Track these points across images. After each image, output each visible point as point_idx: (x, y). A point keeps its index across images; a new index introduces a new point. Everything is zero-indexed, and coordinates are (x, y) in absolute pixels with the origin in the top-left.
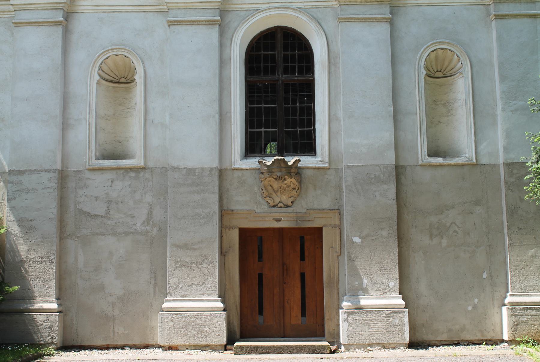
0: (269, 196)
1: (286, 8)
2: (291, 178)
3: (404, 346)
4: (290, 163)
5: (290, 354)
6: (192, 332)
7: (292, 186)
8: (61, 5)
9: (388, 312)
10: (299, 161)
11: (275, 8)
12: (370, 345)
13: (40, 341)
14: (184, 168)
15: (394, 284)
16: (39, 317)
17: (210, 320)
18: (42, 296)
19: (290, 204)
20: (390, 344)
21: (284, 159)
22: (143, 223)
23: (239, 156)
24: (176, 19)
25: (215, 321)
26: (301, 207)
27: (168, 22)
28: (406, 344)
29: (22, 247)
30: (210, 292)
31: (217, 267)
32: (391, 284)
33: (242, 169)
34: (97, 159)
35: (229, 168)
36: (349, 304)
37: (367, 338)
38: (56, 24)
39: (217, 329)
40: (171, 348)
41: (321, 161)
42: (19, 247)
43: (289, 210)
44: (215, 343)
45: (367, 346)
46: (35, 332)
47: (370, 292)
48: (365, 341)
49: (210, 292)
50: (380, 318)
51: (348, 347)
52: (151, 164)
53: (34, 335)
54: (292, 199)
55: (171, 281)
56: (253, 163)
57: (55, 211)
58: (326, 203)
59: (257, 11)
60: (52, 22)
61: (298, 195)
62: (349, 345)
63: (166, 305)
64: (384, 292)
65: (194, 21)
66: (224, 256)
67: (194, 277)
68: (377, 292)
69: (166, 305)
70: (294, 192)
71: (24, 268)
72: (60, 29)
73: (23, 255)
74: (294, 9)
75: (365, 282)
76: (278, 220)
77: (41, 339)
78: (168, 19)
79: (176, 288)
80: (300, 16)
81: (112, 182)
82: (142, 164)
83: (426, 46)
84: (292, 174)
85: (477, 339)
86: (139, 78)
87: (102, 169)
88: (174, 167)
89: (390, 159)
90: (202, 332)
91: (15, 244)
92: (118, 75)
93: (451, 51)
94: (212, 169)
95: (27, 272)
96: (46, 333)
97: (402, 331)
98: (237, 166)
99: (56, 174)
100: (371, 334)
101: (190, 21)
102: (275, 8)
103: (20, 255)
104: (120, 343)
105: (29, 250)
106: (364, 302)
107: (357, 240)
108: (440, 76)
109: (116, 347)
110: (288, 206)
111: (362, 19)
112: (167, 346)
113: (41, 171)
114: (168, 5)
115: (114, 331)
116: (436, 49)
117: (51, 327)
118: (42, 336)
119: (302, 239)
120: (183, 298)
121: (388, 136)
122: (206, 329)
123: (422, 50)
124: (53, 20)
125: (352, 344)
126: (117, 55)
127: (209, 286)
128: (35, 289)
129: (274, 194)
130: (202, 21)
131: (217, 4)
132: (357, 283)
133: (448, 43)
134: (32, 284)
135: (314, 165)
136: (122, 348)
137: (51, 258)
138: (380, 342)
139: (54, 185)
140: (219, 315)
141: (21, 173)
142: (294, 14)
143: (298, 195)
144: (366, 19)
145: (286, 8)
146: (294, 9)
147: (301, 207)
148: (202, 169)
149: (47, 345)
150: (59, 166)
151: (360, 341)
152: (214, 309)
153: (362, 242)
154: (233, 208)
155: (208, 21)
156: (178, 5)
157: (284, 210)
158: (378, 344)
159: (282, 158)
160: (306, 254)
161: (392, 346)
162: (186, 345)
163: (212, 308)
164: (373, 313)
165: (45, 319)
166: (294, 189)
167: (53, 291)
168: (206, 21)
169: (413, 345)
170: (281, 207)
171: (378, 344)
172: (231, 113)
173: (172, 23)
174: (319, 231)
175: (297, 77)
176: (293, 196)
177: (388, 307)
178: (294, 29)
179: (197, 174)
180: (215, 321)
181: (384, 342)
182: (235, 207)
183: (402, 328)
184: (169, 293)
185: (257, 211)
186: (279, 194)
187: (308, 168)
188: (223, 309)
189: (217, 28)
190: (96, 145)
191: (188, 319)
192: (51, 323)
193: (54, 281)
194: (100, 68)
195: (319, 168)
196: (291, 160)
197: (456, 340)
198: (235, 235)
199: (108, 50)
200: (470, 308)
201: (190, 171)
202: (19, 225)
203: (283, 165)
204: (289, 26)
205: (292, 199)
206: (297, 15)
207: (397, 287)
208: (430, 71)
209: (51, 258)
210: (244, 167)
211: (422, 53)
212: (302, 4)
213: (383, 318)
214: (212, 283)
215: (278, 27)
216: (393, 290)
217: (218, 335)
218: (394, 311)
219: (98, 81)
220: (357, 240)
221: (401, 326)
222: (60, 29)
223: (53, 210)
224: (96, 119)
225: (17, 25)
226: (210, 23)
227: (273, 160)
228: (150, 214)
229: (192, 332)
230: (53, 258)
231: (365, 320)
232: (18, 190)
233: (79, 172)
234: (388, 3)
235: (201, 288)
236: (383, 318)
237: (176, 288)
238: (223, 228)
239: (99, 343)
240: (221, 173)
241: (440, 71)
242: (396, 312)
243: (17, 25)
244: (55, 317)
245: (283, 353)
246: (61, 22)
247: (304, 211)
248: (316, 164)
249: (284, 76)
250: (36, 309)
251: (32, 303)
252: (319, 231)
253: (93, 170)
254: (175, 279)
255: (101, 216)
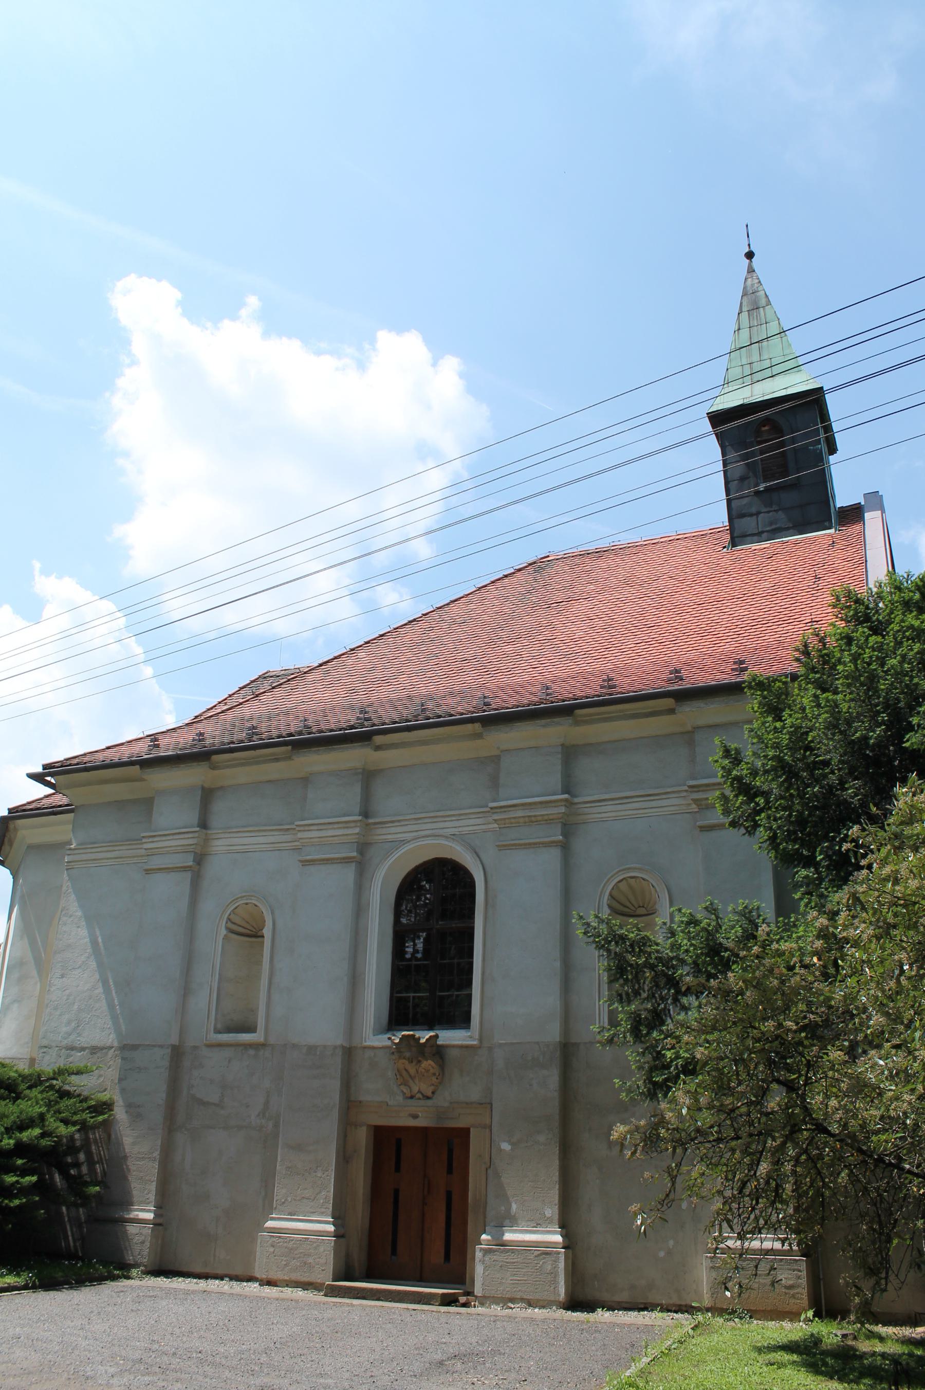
0: (405, 1084)
1: (436, 836)
2: (427, 1060)
3: (557, 1306)
4: (423, 1041)
5: (390, 1301)
6: (294, 1263)
7: (432, 1071)
8: (192, 847)
9: (536, 1253)
10: (437, 1036)
11: (423, 837)
12: (512, 1300)
13: (129, 1260)
14: (305, 1046)
15: (552, 1211)
16: (132, 1229)
17: (316, 1248)
18: (140, 1203)
19: (430, 1094)
20: (538, 1300)
21: (413, 1036)
22: (258, 1115)
23: (371, 1031)
24: (309, 858)
25: (322, 1249)
26: (443, 1099)
27: (301, 861)
28: (560, 1302)
29: (127, 1138)
30: (323, 1210)
31: (333, 1176)
32: (548, 1213)
33: (373, 1048)
34: (218, 1031)
35: (359, 1045)
36: (489, 1237)
37: (508, 1289)
38: (185, 869)
39: (323, 1261)
40: (270, 1283)
41: (471, 1037)
42: (124, 1138)
43: (429, 1102)
44: (319, 1281)
45: (507, 1301)
46: (126, 1248)
47: (520, 1222)
48: (505, 1293)
49: (323, 1210)
50: (527, 1261)
51: (484, 1301)
52: (272, 1041)
53: (125, 1252)
54: (432, 1087)
55: (279, 1192)
56: (382, 1040)
57: (164, 1095)
58: (475, 1094)
59: (404, 842)
60: (182, 867)
61: (440, 1083)
62: (484, 1297)
63: (270, 1224)
64: (538, 1223)
65: (328, 860)
66: (347, 1162)
67: (306, 1189)
68: (529, 1223)
69: (270, 1224)
70: (434, 1079)
71: (127, 1166)
72: (188, 875)
73: (128, 1149)
74: (446, 837)
75: (514, 1206)
76: (415, 1117)
77: (131, 1258)
78: (301, 858)
79: (284, 1203)
80: (453, 845)
81: (229, 1061)
82: (262, 1040)
83: (612, 874)
84: (426, 1054)
85: (671, 1303)
86: (267, 932)
87: (220, 1045)
88: (293, 1044)
89: (553, 1033)
90: (305, 1263)
91: (121, 1135)
92: (255, 926)
93: (644, 879)
94: (335, 1047)
95: (129, 1170)
96: (137, 1249)
97: (555, 1282)
98: (368, 1043)
99: (169, 1050)
100: (513, 1284)
101: (323, 860)
102: (423, 837)
103: (124, 1149)
104: (220, 1272)
105: (134, 1144)
106: (508, 1236)
107: (506, 1146)
108: (643, 913)
109: (215, 1277)
110: (428, 1098)
111: (525, 844)
112: (265, 1281)
113: (154, 1046)
114: (301, 841)
115: (215, 1256)
116: (624, 879)
117: (143, 1242)
118: (132, 1253)
119: (399, 1143)
120: (292, 1215)
121: (553, 1001)
122: (310, 1260)
123: (606, 880)
124: (181, 865)
125: (489, 1297)
126: (247, 904)
127: (322, 1201)
128: (135, 1193)
129: (411, 1081)
130: (337, 859)
131: (354, 837)
132: (503, 1208)
133: (640, 870)
134: (132, 1186)
135: (460, 1043)
136: (221, 1278)
137: (154, 1155)
138: (525, 1297)
139: (166, 1063)
140: (327, 1242)
141: (135, 1047)
142: (446, 843)
143: (440, 1083)
144: (530, 844)
145: (436, 836)
146: (446, 837)
147: (443, 1099)
148: (325, 1047)
149: (135, 1266)
150: (174, 1040)
151: (498, 1292)
152: (322, 1234)
153: (512, 1149)
154: (361, 1098)
155: (344, 858)
156: (312, 840)
157: (422, 1102)
158: (522, 1300)
159: (411, 1033)
160: (455, 1164)
161: (541, 1303)
162: (286, 1281)
163: (320, 1231)
164: (517, 1253)
165: (137, 1231)
166: (434, 1074)
167: (152, 1197)
168: (341, 859)
169: (575, 1303)
170: (419, 1099)
171: (522, 1300)
172: (365, 974)
173: (306, 863)
174: (464, 1133)
175: (455, 924)
176: (433, 1085)
177: (540, 1245)
178: (455, 861)
179: (318, 1053)
180: (322, 1249)
181: (531, 1297)
182: (365, 1097)
183: (555, 1277)
184: (276, 1208)
185: (389, 1103)
186: (417, 1081)
187: (454, 1046)
188: (333, 1235)
189: (353, 866)
190: (216, 1014)
191: (290, 1245)
192: (143, 1238)
193: (154, 1183)
194: (229, 919)
195: (467, 1047)
196: (424, 1036)
197: (642, 1303)
198: (362, 1138)
199: (237, 899)
200: (662, 1254)
201: (311, 1049)
202: (126, 1112)
203: (412, 1042)
204: (449, 857)
205: (432, 1087)
206: (450, 844)
207: (556, 1217)
208: (628, 907)
209: (154, 1155)
210: (376, 1044)
211: (605, 885)
212: (456, 830)
213: (530, 1261)
214: (326, 1198)
215: (437, 859)
216: (550, 1221)
217: (323, 1270)
218: (545, 1250)
219: (225, 935)
220: (506, 1146)
221: (554, 1274)
222: (188, 875)
223: (161, 1096)
224: (219, 982)
225: (148, 871)
226: (346, 861)
227: (427, 1037)
228: (267, 1103)
229: (294, 1263)
230: (156, 1154)
231: (507, 1263)
232: (130, 1069)
233: (195, 1048)
234: (558, 821)
235: (312, 1204)
236: (530, 1261)
237: (284, 1203)
238: (347, 1123)
239: (198, 1269)
240: (349, 1053)
241: (643, 907)
242: (547, 1253)
243: (148, 871)
244: (148, 1230)
245: (382, 1300)
246: (190, 867)
247: (446, 1104)
248: (464, 1040)
249: (440, 923)
250: (130, 1218)
251: (129, 1211)
252: (464, 1133)
253: (210, 1046)
254: (284, 1191)
255: (215, 1104)
